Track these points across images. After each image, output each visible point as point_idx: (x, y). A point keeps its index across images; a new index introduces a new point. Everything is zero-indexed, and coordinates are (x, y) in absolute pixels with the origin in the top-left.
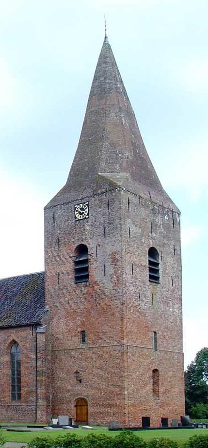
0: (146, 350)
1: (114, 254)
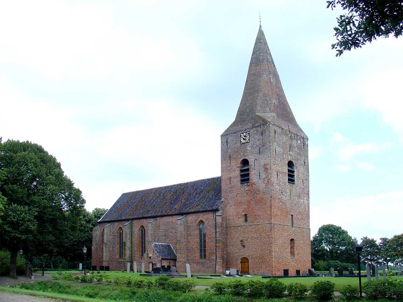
0: (286, 227)
1: (265, 165)
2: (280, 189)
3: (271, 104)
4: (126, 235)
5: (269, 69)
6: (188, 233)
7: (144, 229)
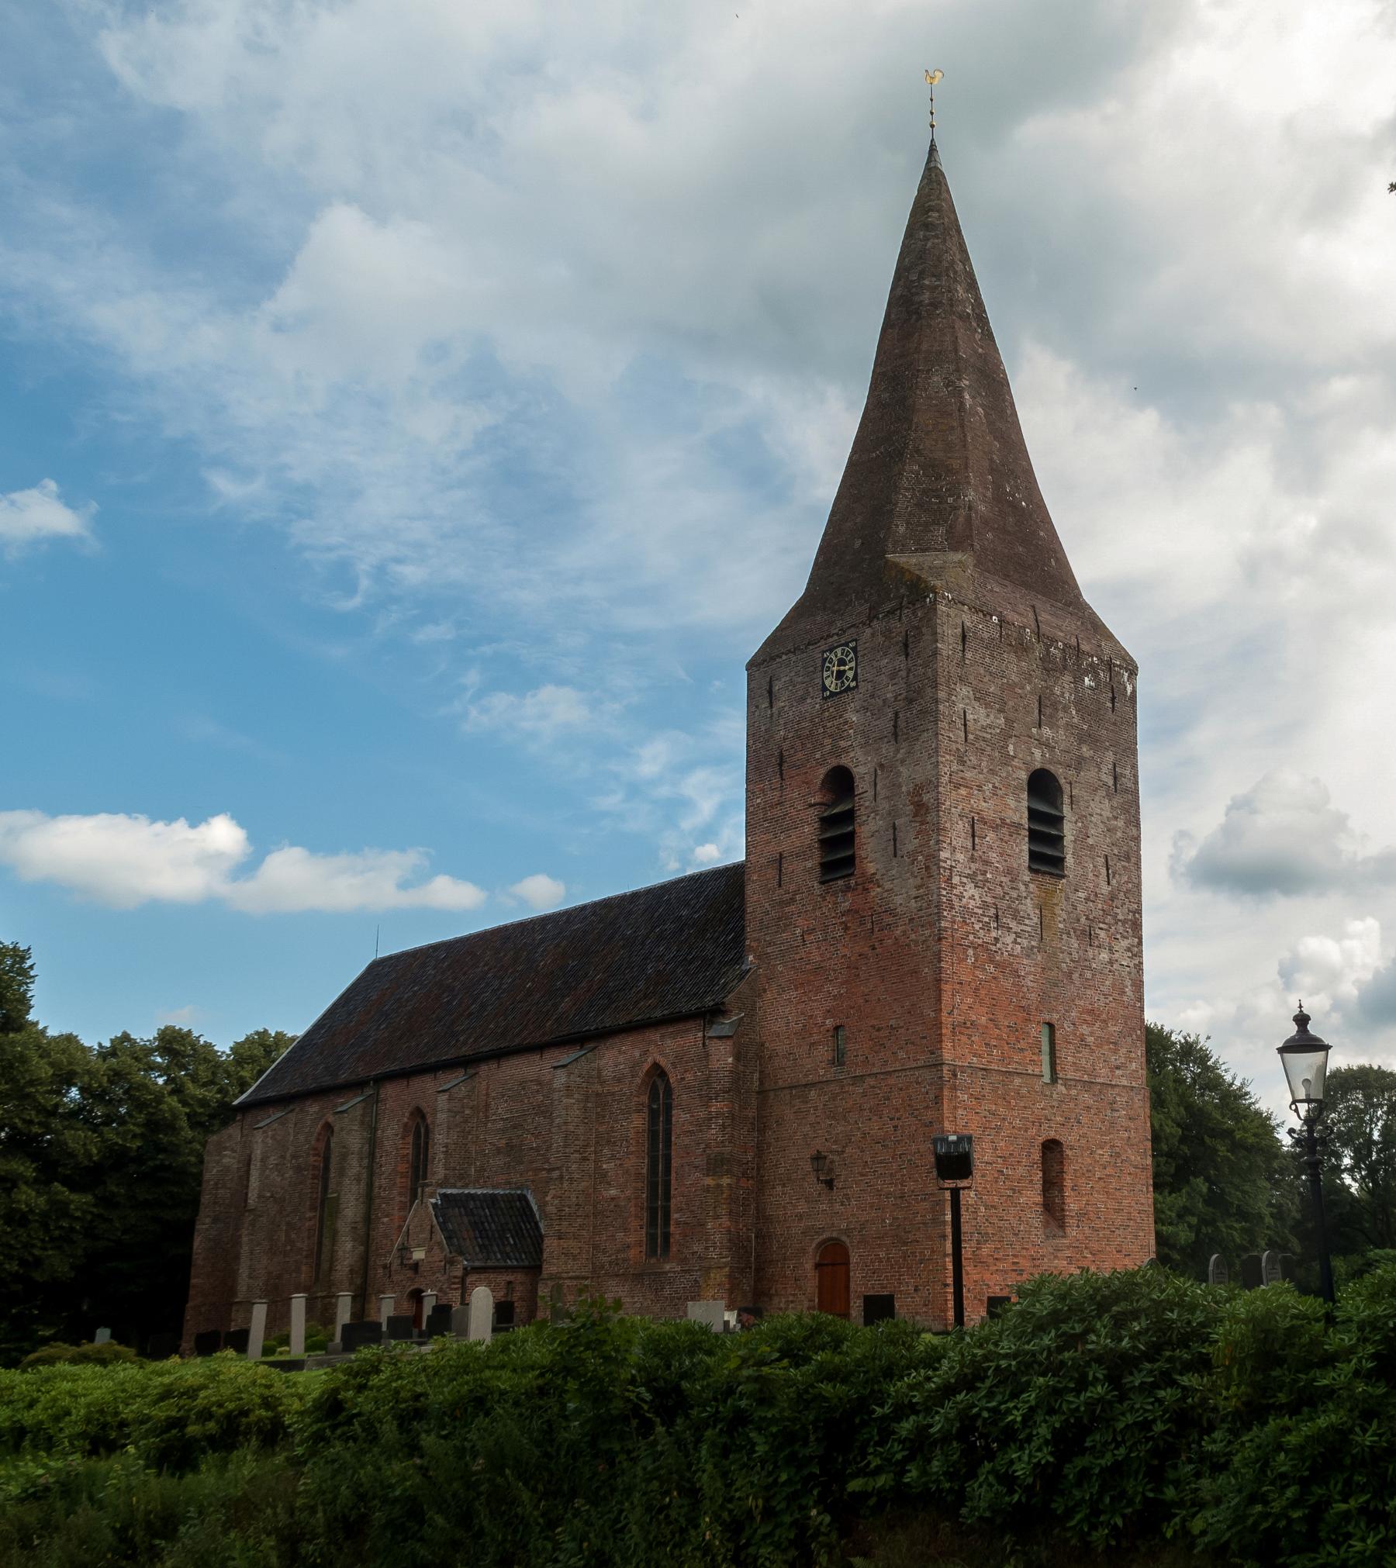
0: (1017, 1081)
2: (989, 900)
3: (955, 508)
4: (344, 1157)
5: (956, 351)
6: (602, 1129)
7: (427, 1126)
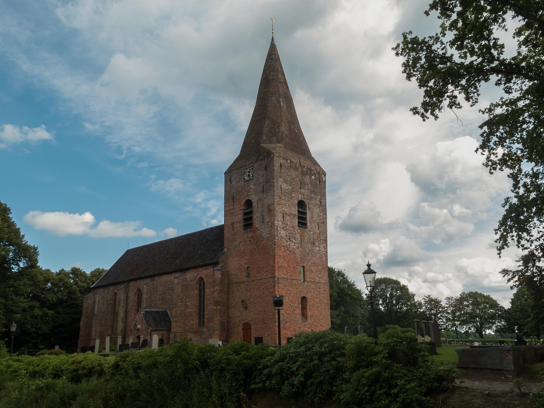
0: (295, 281)
1: (269, 205)
4: (120, 301)
6: (187, 294)
